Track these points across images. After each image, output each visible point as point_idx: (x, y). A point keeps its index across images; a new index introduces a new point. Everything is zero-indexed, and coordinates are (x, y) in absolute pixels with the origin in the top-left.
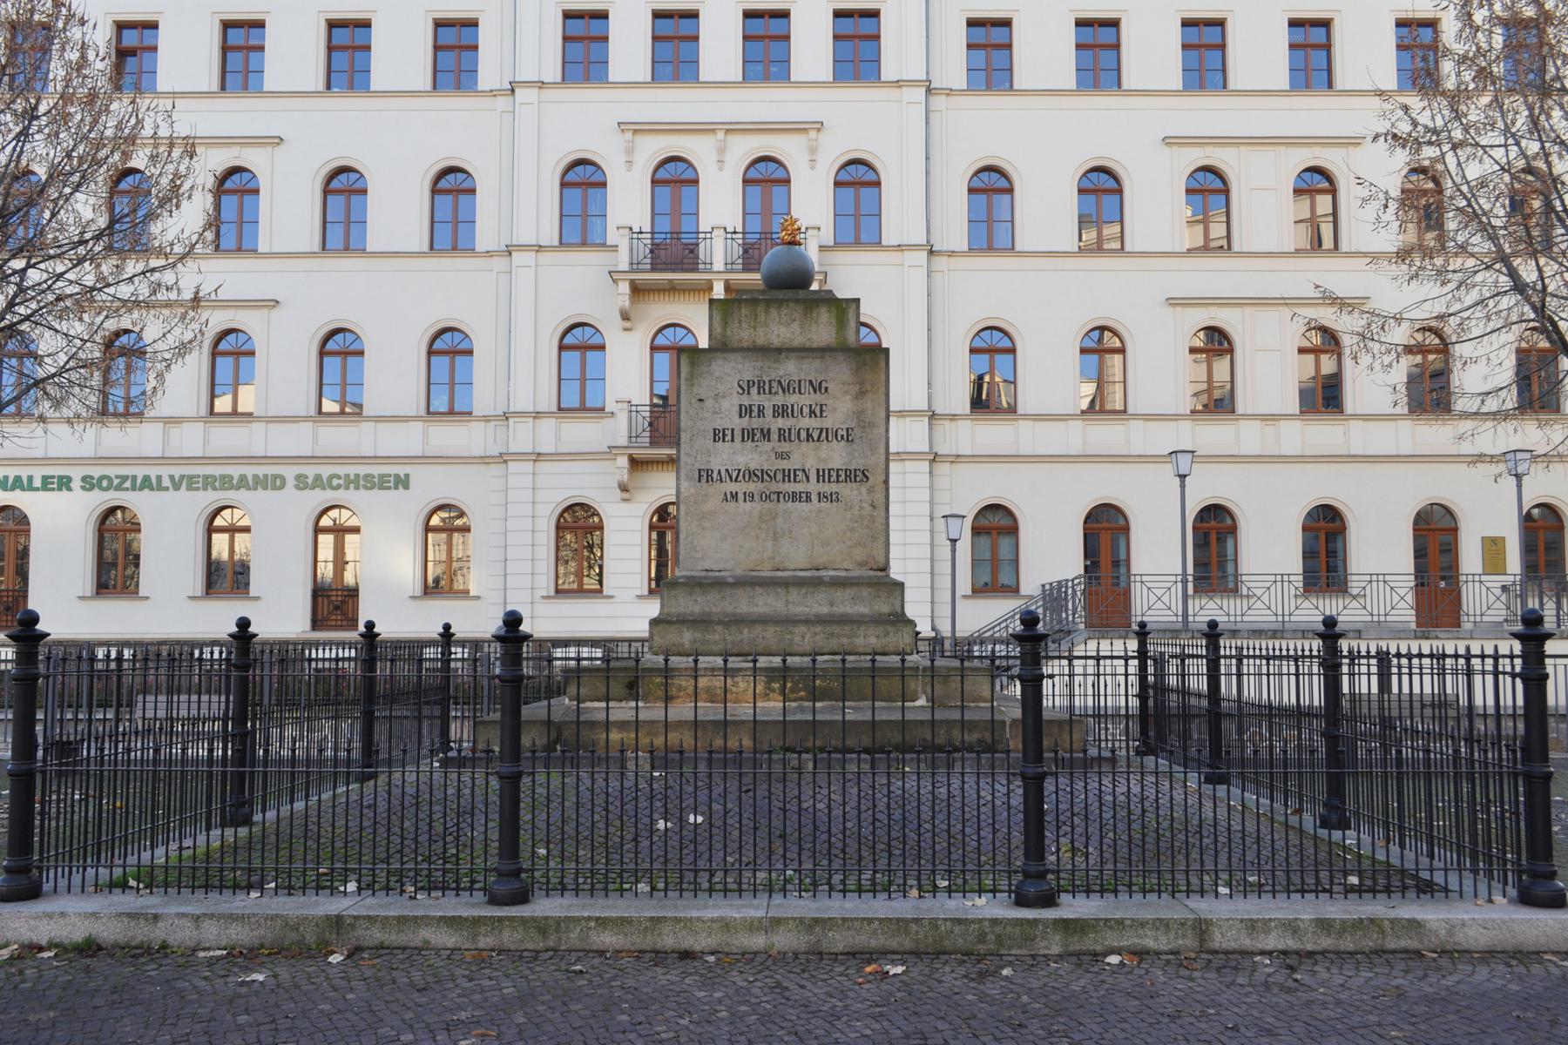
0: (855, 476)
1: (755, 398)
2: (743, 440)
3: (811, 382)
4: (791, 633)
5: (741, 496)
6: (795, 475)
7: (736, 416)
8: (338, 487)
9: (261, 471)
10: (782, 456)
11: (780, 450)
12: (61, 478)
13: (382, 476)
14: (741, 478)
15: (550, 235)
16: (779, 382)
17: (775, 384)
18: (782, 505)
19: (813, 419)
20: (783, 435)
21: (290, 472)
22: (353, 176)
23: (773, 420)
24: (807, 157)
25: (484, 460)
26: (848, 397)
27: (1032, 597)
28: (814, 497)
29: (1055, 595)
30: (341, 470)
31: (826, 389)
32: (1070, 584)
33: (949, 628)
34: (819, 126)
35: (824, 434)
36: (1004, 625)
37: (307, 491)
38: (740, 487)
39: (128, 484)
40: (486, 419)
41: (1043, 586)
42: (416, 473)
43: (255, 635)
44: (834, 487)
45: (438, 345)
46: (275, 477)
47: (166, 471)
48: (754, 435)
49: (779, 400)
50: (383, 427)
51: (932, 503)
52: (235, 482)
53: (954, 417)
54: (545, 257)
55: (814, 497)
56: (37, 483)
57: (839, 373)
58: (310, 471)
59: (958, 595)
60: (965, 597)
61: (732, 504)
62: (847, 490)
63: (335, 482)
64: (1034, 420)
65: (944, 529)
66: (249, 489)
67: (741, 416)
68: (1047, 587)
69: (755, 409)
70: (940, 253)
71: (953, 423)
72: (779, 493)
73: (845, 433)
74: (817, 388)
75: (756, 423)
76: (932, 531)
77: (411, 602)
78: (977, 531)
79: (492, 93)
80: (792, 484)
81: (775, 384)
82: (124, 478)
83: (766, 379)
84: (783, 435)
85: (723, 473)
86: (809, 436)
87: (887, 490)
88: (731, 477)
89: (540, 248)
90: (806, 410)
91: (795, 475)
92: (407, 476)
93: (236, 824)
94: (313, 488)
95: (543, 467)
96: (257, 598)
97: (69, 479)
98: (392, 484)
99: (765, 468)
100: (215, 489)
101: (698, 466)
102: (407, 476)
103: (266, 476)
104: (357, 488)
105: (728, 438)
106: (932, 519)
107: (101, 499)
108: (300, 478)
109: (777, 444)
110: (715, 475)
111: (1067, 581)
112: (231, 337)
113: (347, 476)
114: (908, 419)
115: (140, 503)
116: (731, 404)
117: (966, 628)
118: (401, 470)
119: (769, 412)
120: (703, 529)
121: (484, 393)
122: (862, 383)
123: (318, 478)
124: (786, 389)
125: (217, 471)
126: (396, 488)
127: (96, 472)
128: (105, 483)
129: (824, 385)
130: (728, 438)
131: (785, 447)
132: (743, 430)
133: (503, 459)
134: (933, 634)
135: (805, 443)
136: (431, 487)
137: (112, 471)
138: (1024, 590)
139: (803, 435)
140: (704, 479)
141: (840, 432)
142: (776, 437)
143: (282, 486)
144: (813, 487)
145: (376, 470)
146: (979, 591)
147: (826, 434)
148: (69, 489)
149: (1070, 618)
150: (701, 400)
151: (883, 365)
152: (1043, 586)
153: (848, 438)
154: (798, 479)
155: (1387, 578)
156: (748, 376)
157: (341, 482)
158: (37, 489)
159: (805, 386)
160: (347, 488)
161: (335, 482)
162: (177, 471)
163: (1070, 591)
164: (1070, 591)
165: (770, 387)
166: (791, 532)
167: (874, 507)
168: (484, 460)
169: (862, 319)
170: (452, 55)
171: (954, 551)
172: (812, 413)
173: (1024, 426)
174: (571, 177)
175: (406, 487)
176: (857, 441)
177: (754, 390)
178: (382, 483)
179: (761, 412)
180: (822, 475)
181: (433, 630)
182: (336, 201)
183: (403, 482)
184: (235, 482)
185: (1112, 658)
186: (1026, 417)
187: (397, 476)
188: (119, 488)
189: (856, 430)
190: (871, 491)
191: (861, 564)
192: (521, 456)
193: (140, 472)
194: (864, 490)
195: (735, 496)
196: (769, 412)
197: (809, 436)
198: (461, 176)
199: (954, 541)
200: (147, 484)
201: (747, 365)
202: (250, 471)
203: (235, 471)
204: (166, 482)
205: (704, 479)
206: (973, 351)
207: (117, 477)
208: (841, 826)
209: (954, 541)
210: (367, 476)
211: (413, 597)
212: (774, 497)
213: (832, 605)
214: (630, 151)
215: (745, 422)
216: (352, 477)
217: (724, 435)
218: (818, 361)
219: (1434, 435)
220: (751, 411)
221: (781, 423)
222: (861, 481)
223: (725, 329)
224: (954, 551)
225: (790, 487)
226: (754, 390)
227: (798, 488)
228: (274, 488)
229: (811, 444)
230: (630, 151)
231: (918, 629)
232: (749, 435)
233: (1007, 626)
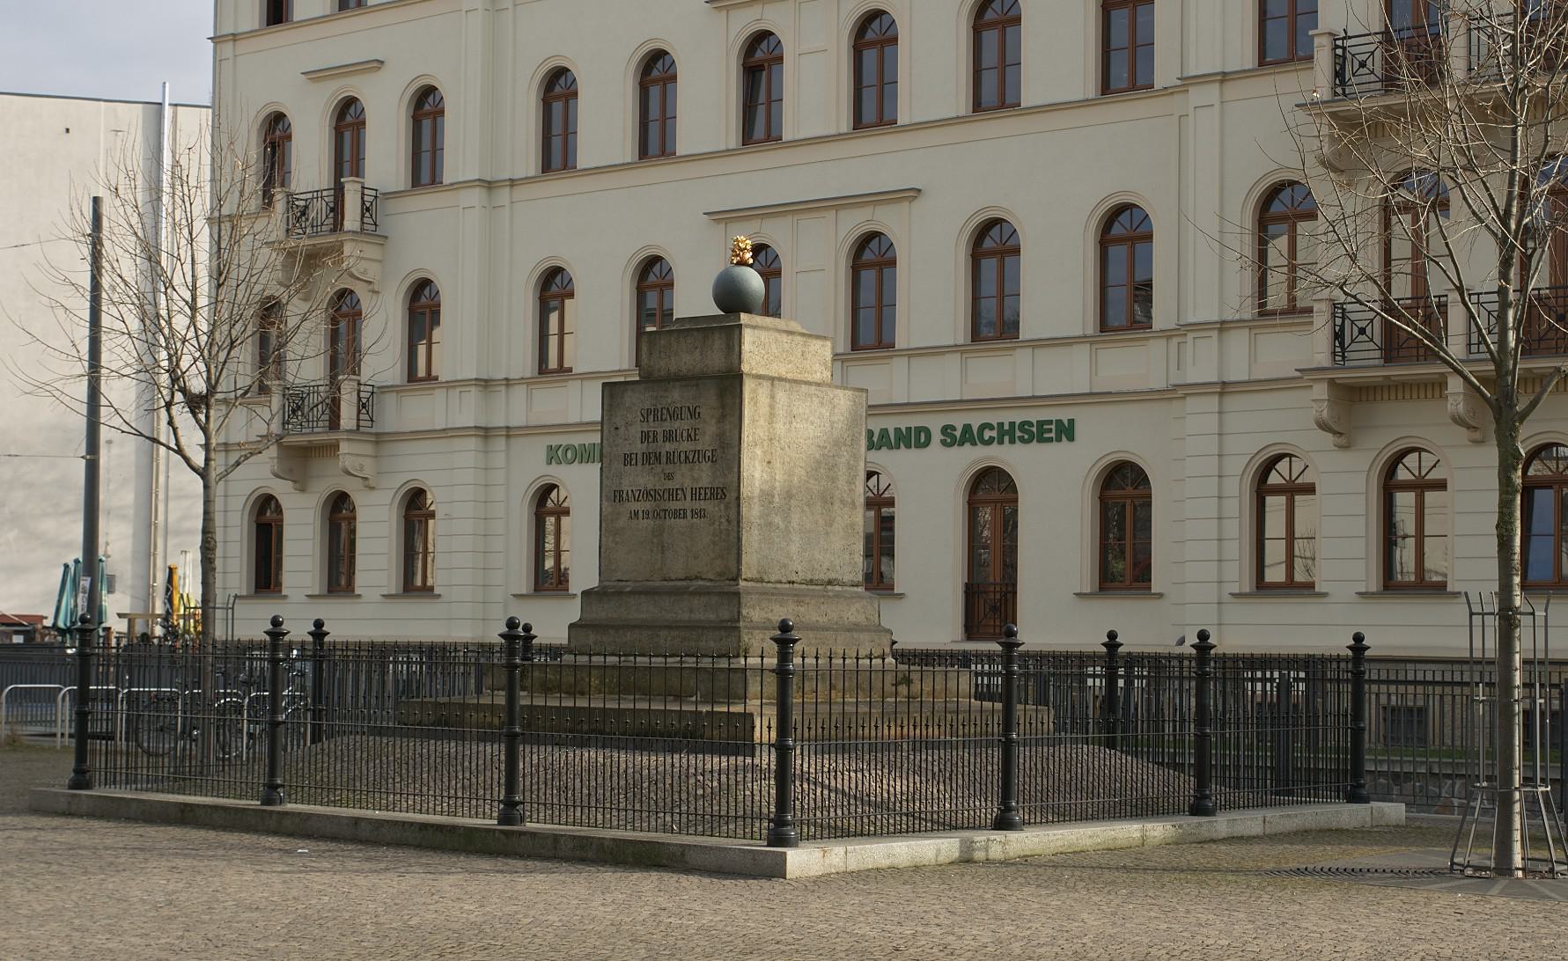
1: (652, 426)
4: (658, 636)
7: (639, 442)
8: (990, 441)
9: (904, 423)
11: (667, 472)
13: (1041, 424)
15: (1243, 53)
30: (993, 418)
42: (1086, 420)
43: (1019, 645)
44: (703, 504)
46: (919, 430)
49: (667, 426)
50: (1043, 354)
54: (1234, 89)
57: (708, 400)
58: (958, 421)
63: (987, 434)
66: (891, 447)
74: (694, 414)
81: (665, 412)
83: (659, 407)
85: (630, 493)
87: (739, 506)
89: (1224, 77)
90: (685, 434)
92: (1071, 422)
94: (961, 444)
95: (1233, 402)
96: (901, 596)
98: (1053, 435)
102: (1071, 422)
103: (908, 429)
104: (1012, 441)
108: (948, 430)
113: (1001, 425)
116: (636, 430)
118: (1063, 415)
120: (616, 543)
122: (723, 407)
123: (967, 428)
126: (1059, 440)
131: (669, 469)
143: (927, 444)
145: (1034, 416)
150: (617, 428)
154: (679, 497)
157: (994, 434)
159: (685, 414)
160: (1001, 442)
161: (987, 434)
175: (1071, 438)
176: (719, 461)
180: (696, 494)
181: (1094, 642)
183: (1066, 431)
187: (1059, 422)
190: (727, 507)
192: (1199, 389)
194: (722, 507)
195: (636, 513)
210: (1023, 424)
212: (662, 514)
213: (691, 611)
217: (631, 459)
219: (862, 475)
220: (649, 437)
221: (668, 447)
223: (649, 360)
225: (673, 505)
228: (919, 445)
229: (688, 465)
231: (894, 638)
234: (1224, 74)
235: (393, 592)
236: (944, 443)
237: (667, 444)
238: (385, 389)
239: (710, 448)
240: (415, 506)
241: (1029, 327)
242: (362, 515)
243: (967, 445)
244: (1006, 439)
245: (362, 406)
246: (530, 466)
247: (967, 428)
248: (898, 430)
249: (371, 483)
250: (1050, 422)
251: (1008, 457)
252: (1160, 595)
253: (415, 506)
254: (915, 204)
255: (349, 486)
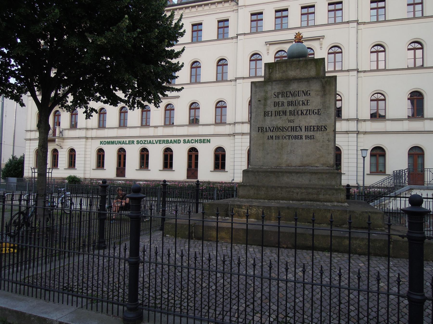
0: (321, 128)
1: (281, 99)
2: (275, 115)
3: (303, 91)
5: (274, 137)
6: (296, 129)
7: (273, 106)
10: (290, 121)
11: (290, 119)
12: (132, 141)
13: (203, 140)
14: (274, 130)
16: (290, 92)
17: (288, 93)
18: (291, 141)
19: (304, 106)
20: (292, 113)
21: (182, 139)
22: (198, 63)
23: (288, 107)
24: (319, 47)
25: (229, 135)
26: (319, 97)
27: (389, 175)
28: (304, 137)
29: (397, 175)
30: (194, 138)
31: (309, 94)
32: (404, 171)
33: (362, 183)
34: (323, 37)
35: (308, 112)
36: (381, 183)
37: (186, 144)
38: (274, 134)
39: (146, 142)
40: (230, 124)
41: (394, 171)
44: (312, 133)
45: (218, 105)
46: (178, 140)
47: (154, 139)
48: (280, 113)
49: (290, 99)
51: (357, 146)
52: (169, 142)
53: (365, 121)
55: (304, 137)
56: (127, 142)
59: (365, 174)
60: (367, 174)
61: (270, 141)
62: (318, 135)
63: (192, 141)
64: (391, 121)
65: (361, 154)
67: (275, 106)
68: (395, 172)
69: (281, 103)
70: (361, 72)
71: (365, 122)
72: (289, 136)
73: (317, 111)
74: (306, 93)
75: (281, 109)
76: (357, 154)
77: (211, 172)
78: (372, 155)
79: (232, 38)
80: (295, 132)
82: (145, 141)
84: (291, 113)
85: (268, 128)
86: (302, 113)
88: (270, 130)
91: (296, 129)
92: (210, 139)
93: (99, 248)
96: (174, 171)
97: (134, 141)
98: (206, 142)
99: (284, 126)
100: (165, 143)
101: (258, 126)
104: (198, 143)
105: (270, 115)
106: (357, 151)
107: (141, 146)
108: (184, 140)
109: (289, 116)
110: (264, 129)
111: (402, 170)
112: (169, 106)
114: (350, 121)
115: (149, 147)
117: (367, 184)
118: (208, 138)
119: (286, 104)
121: (229, 118)
124: (293, 95)
125: (166, 139)
127: (140, 140)
128: (141, 142)
129: (309, 92)
130: (270, 115)
131: (292, 118)
132: (276, 111)
133: (234, 135)
134: (357, 185)
135: (300, 116)
136: (216, 143)
137: (143, 139)
138: (387, 173)
139: (300, 112)
140: (260, 131)
141: (315, 111)
142: (289, 114)
143: (180, 143)
144: (303, 133)
146: (372, 173)
147: (310, 112)
148: (134, 144)
149: (404, 182)
151: (334, 87)
152: (394, 171)
153: (318, 113)
155: (431, 170)
156: (277, 91)
158: (127, 144)
161: (192, 141)
162: (157, 139)
163: (404, 174)
164: (404, 174)
165: (287, 94)
166: (294, 151)
167: (329, 141)
168: (229, 135)
169: (337, 93)
170: (222, 29)
171: (364, 160)
172: (303, 103)
173: (388, 123)
174: (252, 58)
177: (280, 96)
178: (204, 141)
179: (283, 104)
180: (307, 129)
182: (194, 70)
183: (209, 141)
184: (169, 142)
185: (427, 198)
186: (389, 120)
188: (144, 143)
189: (322, 110)
191: (323, 165)
192: (238, 134)
193: (149, 139)
195: (272, 137)
196: (286, 104)
197: (302, 113)
198: (224, 61)
199: (364, 157)
200: (150, 142)
201: (277, 86)
202: (173, 139)
203: (169, 139)
204: (154, 142)
205: (260, 131)
206: (372, 100)
207: (144, 141)
208: (302, 293)
209: (364, 157)
211: (211, 171)
212: (287, 137)
214: (268, 50)
215: (276, 109)
216: (196, 140)
218: (306, 83)
220: (279, 104)
221: (291, 108)
222: (324, 130)
224: (364, 160)
226: (280, 96)
227: (297, 134)
228: (178, 143)
230: (268, 50)
232: (278, 113)
233: (382, 184)
234: (244, 78)
235: (66, 168)
236: (184, 143)
237: (290, 107)
238: (65, 129)
239: (317, 108)
240: (72, 153)
241: (201, 121)
242: (59, 153)
243: (188, 143)
244: (196, 142)
245: (61, 132)
246: (96, 145)
247: (188, 140)
248: (174, 140)
249: (62, 147)
250: (205, 139)
251: (197, 146)
252: (227, 172)
253: (72, 153)
254: (179, 99)
255: (57, 147)
